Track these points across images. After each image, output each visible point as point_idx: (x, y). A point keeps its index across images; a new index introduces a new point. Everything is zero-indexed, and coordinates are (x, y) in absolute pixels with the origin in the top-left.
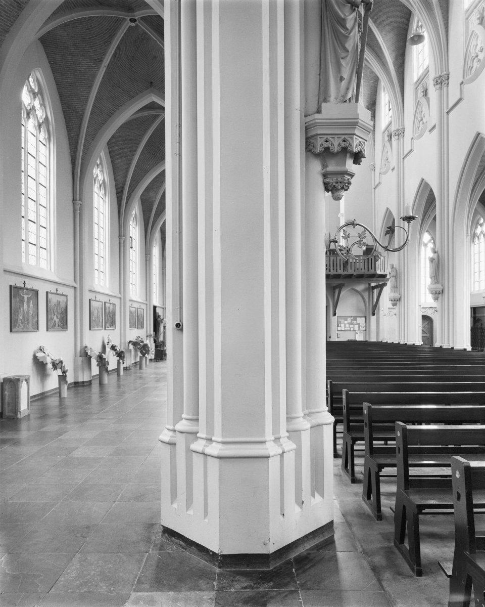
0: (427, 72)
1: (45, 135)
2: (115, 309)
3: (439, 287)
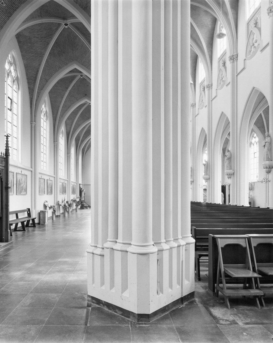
0: (224, 54)
2: (66, 185)
3: (207, 177)
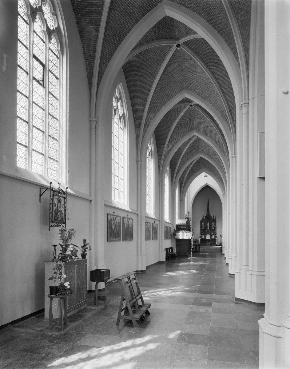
1: (123, 124)
